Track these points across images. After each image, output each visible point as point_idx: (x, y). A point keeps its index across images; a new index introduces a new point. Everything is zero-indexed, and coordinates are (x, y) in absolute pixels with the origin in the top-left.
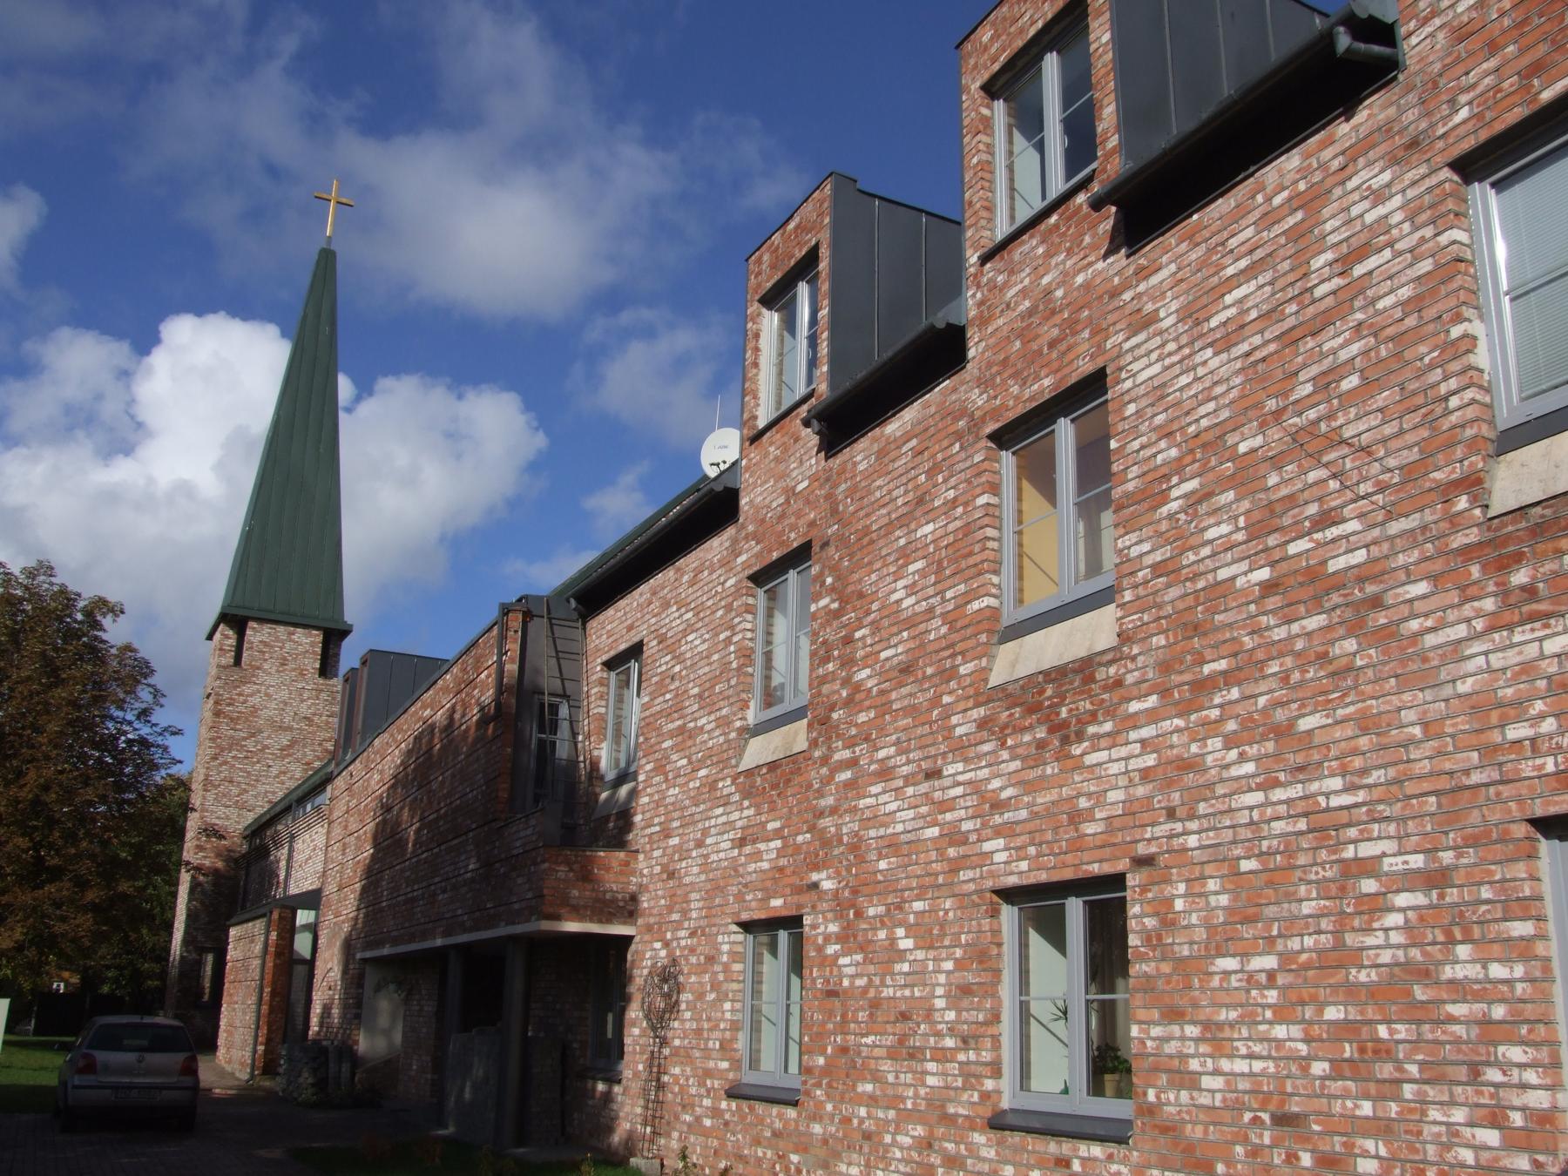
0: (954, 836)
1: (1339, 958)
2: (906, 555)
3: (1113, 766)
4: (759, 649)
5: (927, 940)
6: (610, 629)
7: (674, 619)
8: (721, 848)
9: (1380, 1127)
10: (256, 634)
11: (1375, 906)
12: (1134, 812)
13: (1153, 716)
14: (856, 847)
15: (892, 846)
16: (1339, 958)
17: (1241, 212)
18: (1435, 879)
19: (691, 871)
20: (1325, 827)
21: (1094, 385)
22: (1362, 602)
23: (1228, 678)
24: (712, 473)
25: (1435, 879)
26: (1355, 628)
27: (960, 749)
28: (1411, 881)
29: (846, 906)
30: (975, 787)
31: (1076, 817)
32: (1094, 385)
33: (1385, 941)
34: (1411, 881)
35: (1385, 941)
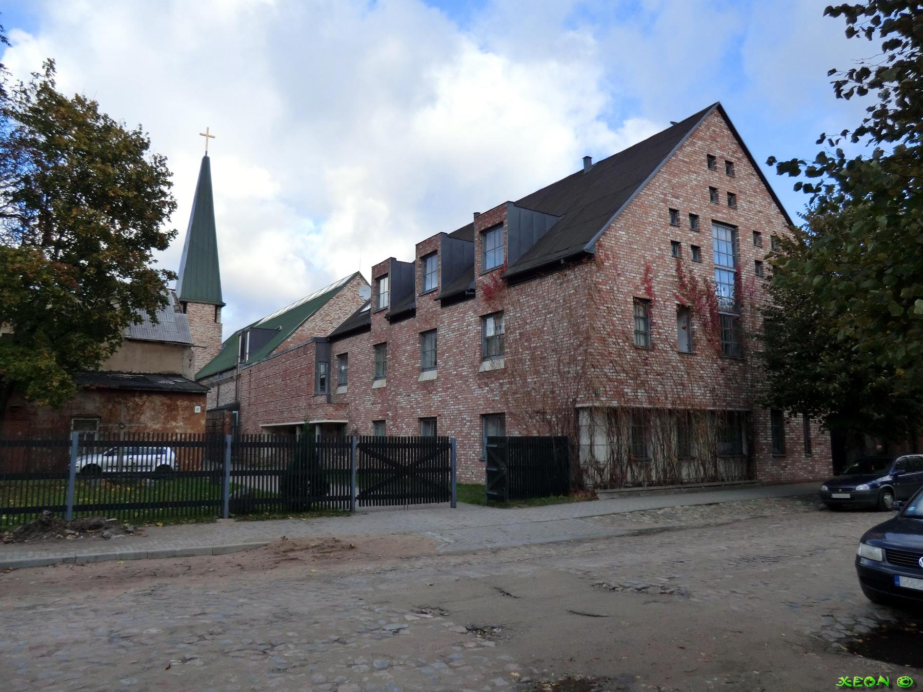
0: (412, 407)
1: (461, 431)
2: (405, 351)
3: (436, 398)
4: (675, 523)
5: (408, 426)
6: (340, 347)
7: (355, 350)
8: (368, 405)
9: (464, 455)
10: (191, 308)
11: (465, 424)
12: (438, 407)
13: (441, 392)
14: (396, 408)
15: (402, 408)
16: (461, 431)
17: (456, 309)
18: (471, 421)
19: (361, 409)
20: (460, 413)
21: (434, 330)
22: (465, 379)
23: (450, 388)
24: (98, 399)
25: (471, 421)
26: (465, 383)
27: (414, 392)
28: (468, 421)
29: (394, 419)
30: (416, 399)
31: (431, 407)
32: (434, 330)
33: (465, 430)
34: (468, 421)
35: (465, 430)
